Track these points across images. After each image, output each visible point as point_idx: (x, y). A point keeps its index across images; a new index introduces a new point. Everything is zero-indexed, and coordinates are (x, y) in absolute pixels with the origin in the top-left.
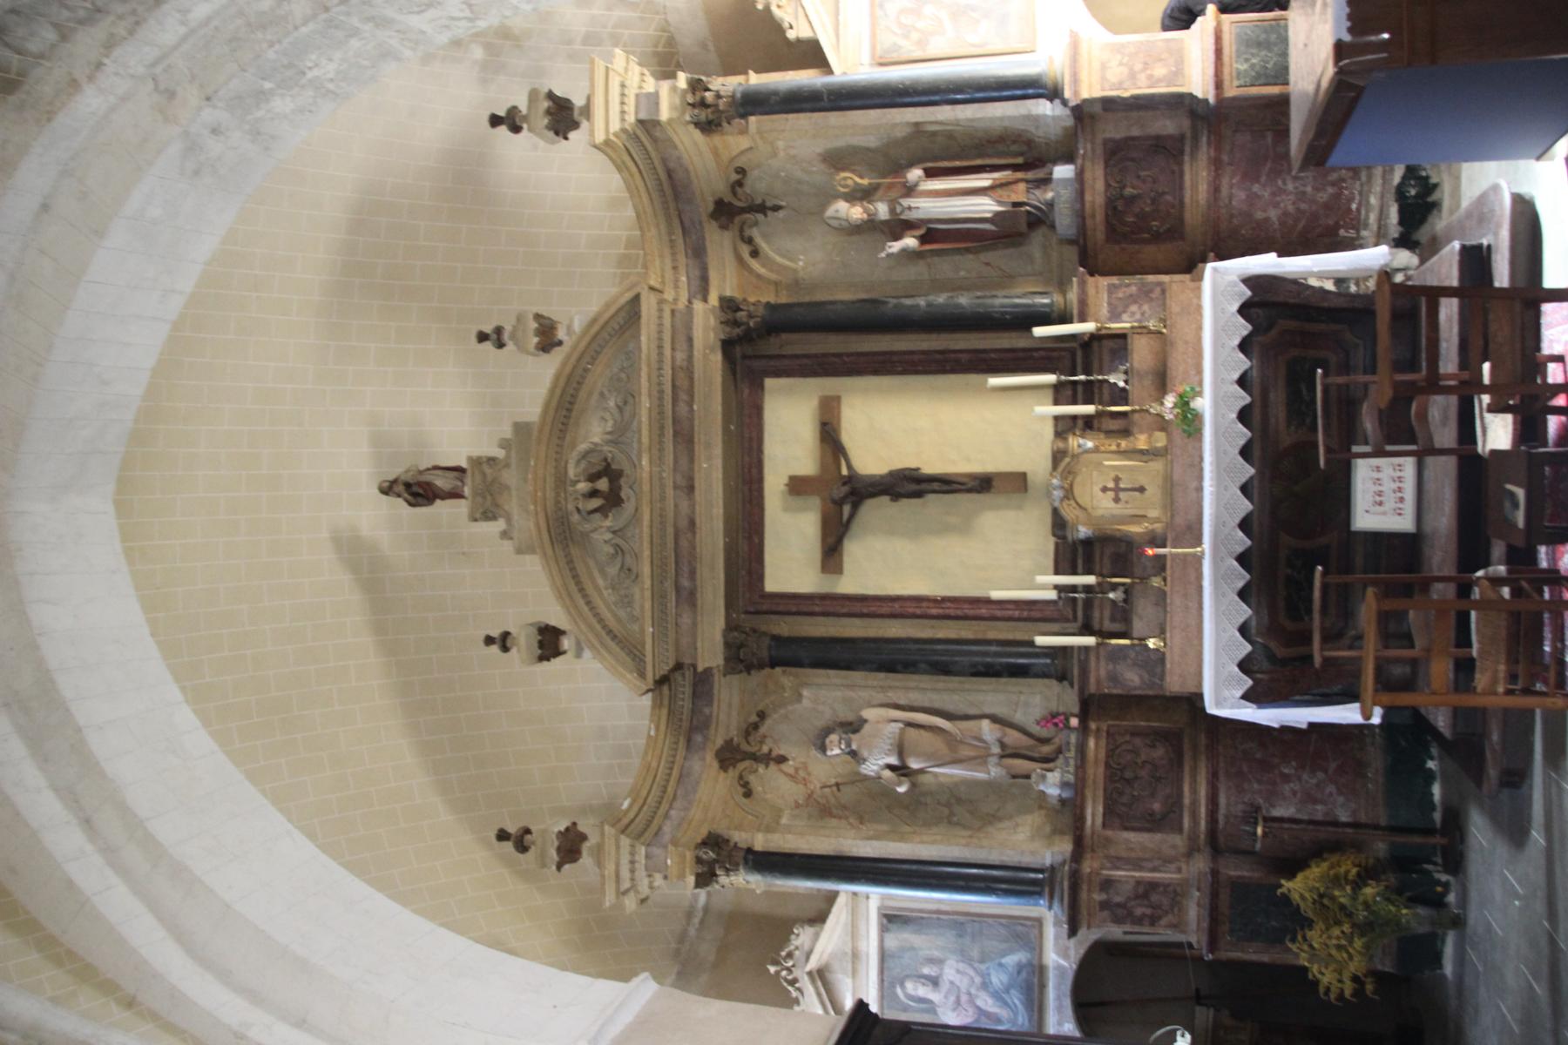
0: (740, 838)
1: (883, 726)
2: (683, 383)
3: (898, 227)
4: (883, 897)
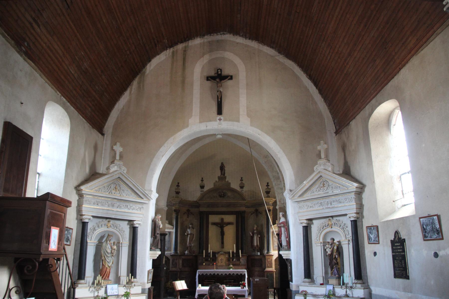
0: (179, 213)
3: (253, 234)
4: (173, 232)
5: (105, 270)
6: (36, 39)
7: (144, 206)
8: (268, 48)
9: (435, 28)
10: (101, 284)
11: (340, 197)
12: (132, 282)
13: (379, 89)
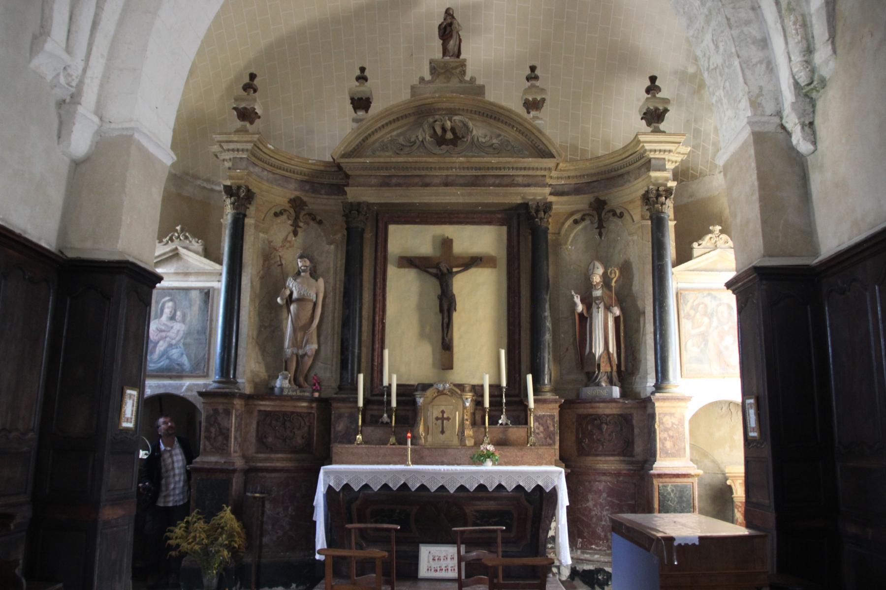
0: (252, 210)
3: (588, 302)
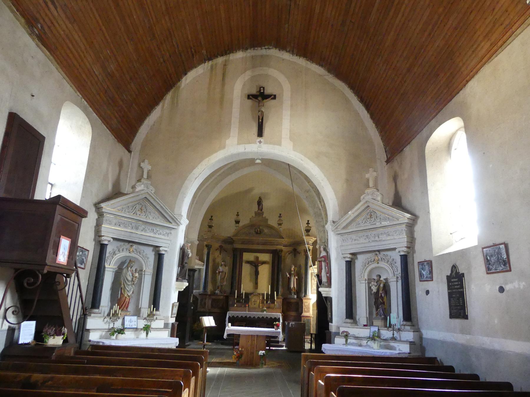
1: (224, 269)
2: (271, 244)
3: (290, 274)
5: (123, 299)
6: (52, 23)
7: (173, 231)
8: (317, 67)
9: (514, 29)
10: (118, 315)
11: (389, 229)
12: (154, 315)
13: (440, 107)
